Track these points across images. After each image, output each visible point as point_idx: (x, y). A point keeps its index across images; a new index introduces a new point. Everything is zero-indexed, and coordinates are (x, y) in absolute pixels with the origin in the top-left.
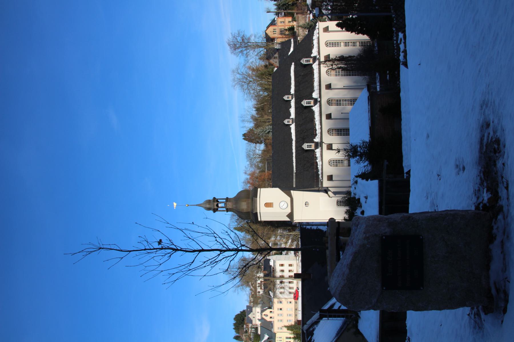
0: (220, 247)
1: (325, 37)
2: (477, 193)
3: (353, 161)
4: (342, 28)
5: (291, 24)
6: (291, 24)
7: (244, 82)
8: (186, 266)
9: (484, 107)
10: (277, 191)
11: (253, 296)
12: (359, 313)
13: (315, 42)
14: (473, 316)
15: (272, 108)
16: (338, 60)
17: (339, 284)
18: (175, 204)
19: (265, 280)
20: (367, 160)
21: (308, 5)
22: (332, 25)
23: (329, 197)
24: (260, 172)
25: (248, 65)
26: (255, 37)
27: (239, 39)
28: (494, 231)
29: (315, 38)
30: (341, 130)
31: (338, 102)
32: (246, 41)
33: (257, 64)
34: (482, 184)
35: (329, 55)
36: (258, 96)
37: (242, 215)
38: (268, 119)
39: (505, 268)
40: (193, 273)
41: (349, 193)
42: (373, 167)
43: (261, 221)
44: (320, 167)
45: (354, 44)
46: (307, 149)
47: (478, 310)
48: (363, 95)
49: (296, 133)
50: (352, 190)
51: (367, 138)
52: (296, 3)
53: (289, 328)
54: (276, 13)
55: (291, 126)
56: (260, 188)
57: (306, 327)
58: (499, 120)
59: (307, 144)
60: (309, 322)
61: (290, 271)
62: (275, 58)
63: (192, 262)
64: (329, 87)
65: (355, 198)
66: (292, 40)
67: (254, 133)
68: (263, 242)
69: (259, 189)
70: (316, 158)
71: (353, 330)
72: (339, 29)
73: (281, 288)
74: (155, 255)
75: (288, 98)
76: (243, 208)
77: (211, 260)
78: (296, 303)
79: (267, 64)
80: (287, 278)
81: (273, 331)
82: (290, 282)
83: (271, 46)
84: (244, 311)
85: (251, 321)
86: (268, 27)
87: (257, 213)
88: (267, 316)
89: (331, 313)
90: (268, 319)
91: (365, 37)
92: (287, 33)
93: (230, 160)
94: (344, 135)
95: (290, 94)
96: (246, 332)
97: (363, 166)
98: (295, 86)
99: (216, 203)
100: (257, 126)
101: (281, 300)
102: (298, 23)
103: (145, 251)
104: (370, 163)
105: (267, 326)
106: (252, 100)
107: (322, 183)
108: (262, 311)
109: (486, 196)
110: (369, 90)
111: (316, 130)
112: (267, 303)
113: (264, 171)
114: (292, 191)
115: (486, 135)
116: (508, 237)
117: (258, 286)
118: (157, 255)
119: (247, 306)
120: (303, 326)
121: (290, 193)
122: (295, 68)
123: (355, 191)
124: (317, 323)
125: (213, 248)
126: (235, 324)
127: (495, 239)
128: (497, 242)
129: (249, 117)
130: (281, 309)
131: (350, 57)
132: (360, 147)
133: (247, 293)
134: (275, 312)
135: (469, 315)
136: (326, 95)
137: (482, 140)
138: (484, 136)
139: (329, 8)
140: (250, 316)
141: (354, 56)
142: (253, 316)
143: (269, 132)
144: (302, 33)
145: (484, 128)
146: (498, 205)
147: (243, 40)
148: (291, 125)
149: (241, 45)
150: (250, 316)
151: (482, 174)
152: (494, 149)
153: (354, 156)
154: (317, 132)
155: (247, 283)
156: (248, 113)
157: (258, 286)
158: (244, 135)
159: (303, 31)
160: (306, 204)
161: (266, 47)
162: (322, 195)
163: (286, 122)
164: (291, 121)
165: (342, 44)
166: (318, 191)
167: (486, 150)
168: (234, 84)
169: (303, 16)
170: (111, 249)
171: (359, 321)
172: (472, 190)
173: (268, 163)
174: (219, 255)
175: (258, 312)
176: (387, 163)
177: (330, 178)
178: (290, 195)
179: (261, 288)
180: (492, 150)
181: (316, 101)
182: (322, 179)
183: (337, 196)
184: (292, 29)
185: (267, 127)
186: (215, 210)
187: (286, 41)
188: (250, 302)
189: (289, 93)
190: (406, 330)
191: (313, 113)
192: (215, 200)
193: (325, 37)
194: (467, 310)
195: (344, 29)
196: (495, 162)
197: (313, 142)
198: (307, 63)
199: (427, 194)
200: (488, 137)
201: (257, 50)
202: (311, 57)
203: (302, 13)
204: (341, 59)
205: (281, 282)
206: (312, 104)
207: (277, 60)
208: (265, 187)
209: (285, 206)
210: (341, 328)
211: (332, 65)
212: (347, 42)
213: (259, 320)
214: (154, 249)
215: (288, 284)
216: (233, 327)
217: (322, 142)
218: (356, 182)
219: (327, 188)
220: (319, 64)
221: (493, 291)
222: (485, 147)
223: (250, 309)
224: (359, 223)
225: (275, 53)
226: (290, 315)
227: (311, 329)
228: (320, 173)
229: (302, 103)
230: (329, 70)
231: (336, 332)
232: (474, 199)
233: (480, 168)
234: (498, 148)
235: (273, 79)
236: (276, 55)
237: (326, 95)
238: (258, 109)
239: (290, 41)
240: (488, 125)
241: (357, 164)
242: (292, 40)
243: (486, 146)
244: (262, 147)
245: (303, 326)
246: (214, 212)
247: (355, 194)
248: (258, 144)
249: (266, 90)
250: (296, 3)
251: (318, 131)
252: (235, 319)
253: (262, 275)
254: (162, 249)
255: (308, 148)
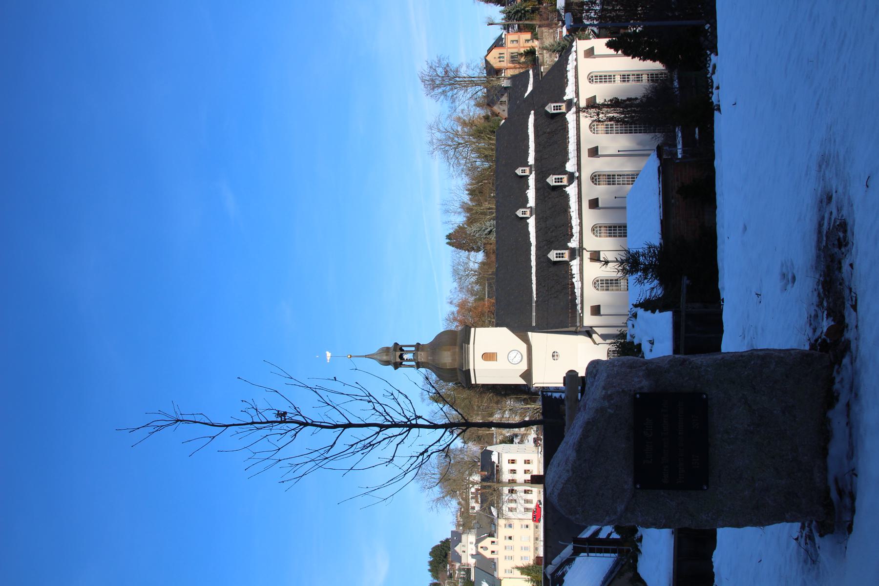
0: (380, 420)
1: (587, 66)
2: (813, 320)
3: (632, 278)
4: (617, 50)
5: (530, 44)
6: (530, 44)
7: (450, 145)
8: (322, 451)
9: (824, 166)
10: (504, 333)
11: (462, 514)
12: (639, 544)
13: (571, 75)
14: (802, 541)
15: (497, 189)
16: (608, 106)
17: (560, 477)
18: (329, 354)
19: (483, 487)
20: (656, 278)
21: (558, 11)
22: (600, 45)
23: (595, 343)
24: (475, 300)
25: (455, 115)
26: (468, 67)
27: (440, 71)
28: (837, 386)
29: (570, 67)
30: (615, 227)
31: (611, 179)
32: (451, 74)
33: (471, 114)
34: (820, 304)
35: (595, 97)
36: (473, 168)
37: (445, 374)
38: (489, 209)
39: (852, 452)
40: (332, 464)
41: (623, 335)
42: (665, 289)
43: (477, 385)
44: (578, 292)
45: (638, 77)
46: (556, 259)
47: (811, 530)
48: (652, 163)
49: (536, 232)
50: (629, 331)
51: (656, 240)
52: (538, 9)
53: (525, 570)
54: (504, 25)
55: (528, 221)
56: (475, 327)
57: (550, 569)
58: (845, 187)
59: (556, 252)
60: (557, 561)
61: (526, 472)
62: (502, 103)
63: (332, 446)
64: (594, 152)
65: (633, 342)
66: (531, 72)
67: (466, 234)
68: (455, 412)
69: (473, 329)
70: (572, 276)
71: (630, 575)
72: (612, 52)
73: (511, 501)
74: (268, 432)
75: (524, 171)
76: (445, 360)
77: (363, 443)
78: (537, 527)
79: (489, 114)
80: (520, 484)
81: (496, 575)
82: (526, 492)
83: (496, 83)
84: (447, 540)
85: (459, 559)
86: (490, 51)
87: (469, 370)
88: (486, 549)
89: (595, 545)
90: (487, 554)
91: (657, 66)
92: (523, 60)
93: (423, 277)
94: (620, 236)
95: (528, 166)
96: (451, 576)
97: (650, 288)
98: (536, 151)
99: (398, 353)
100: (470, 221)
101: (511, 522)
102: (542, 43)
103: (252, 427)
104: (661, 284)
105: (487, 567)
106: (463, 176)
107: (582, 319)
108: (478, 541)
109: (826, 324)
110: (659, 156)
111: (572, 228)
112: (487, 528)
113: (483, 299)
114: (530, 334)
115: (827, 216)
116: (856, 395)
117: (472, 498)
118: (273, 432)
119: (453, 532)
120: (546, 567)
121: (527, 336)
122: (535, 120)
123: (633, 332)
124: (569, 561)
125: (367, 422)
126: (431, 563)
127: (838, 400)
128: (840, 406)
129: (458, 205)
130: (510, 538)
131: (629, 99)
132: (643, 255)
133: (453, 510)
134: (500, 542)
135: (797, 539)
136: (590, 166)
137: (820, 225)
138: (823, 218)
139: (592, 15)
140: (458, 549)
141: (636, 99)
142: (463, 549)
143: (491, 231)
144: (548, 60)
145: (824, 204)
146: (843, 339)
147: (446, 72)
148: (528, 218)
149: (445, 81)
150: (458, 549)
151: (820, 287)
152: (839, 240)
153: (631, 272)
154: (574, 231)
155: (452, 493)
156: (456, 198)
157: (472, 498)
158: (449, 237)
159: (551, 56)
160: (553, 356)
161: (486, 83)
162: (583, 339)
163: (519, 213)
164: (528, 211)
165: (618, 78)
166: (576, 333)
167: (827, 243)
168: (431, 149)
169: (551, 31)
170: (195, 422)
171: (639, 559)
172: (806, 316)
173: (490, 285)
174: (378, 433)
175: (471, 543)
176: (688, 282)
177: (596, 310)
178: (526, 341)
179: (477, 502)
180: (836, 242)
181: (571, 177)
182: (582, 312)
183: (609, 341)
184: (531, 53)
185: (488, 224)
186: (397, 366)
187: (520, 74)
188: (458, 525)
189: (526, 164)
190: (713, 574)
191: (566, 197)
192: (398, 348)
193: (587, 66)
194: (795, 528)
195: (620, 52)
196: (840, 263)
197: (567, 248)
198: (556, 111)
199: (744, 331)
200: (830, 219)
201: (471, 90)
202: (564, 101)
203: (549, 26)
204: (615, 103)
205: (512, 491)
206: (565, 182)
207: (505, 107)
208: (482, 326)
209: (518, 358)
210: (611, 572)
211: (598, 115)
212: (626, 73)
213: (473, 556)
214: (268, 422)
215: (523, 494)
216: (429, 568)
217: (581, 248)
218: (635, 316)
219: (591, 327)
220: (578, 112)
221: (834, 495)
222: (824, 238)
223: (457, 537)
224: (597, 371)
225: (503, 95)
226: (526, 548)
227: (560, 573)
228: (578, 301)
229: (548, 180)
230: (595, 123)
231: (602, 579)
232: (809, 331)
233: (817, 276)
234: (845, 237)
235: (497, 140)
236: (505, 98)
237: (590, 166)
238: (472, 192)
239: (526, 73)
240: (830, 199)
241: (638, 286)
242: (531, 72)
243: (827, 237)
244: (480, 256)
245: (546, 567)
246: (396, 368)
247: (633, 336)
248: (473, 253)
249: (486, 158)
250: (538, 9)
251: (576, 230)
252: (431, 554)
253: (476, 478)
254: (285, 422)
255: (558, 259)
